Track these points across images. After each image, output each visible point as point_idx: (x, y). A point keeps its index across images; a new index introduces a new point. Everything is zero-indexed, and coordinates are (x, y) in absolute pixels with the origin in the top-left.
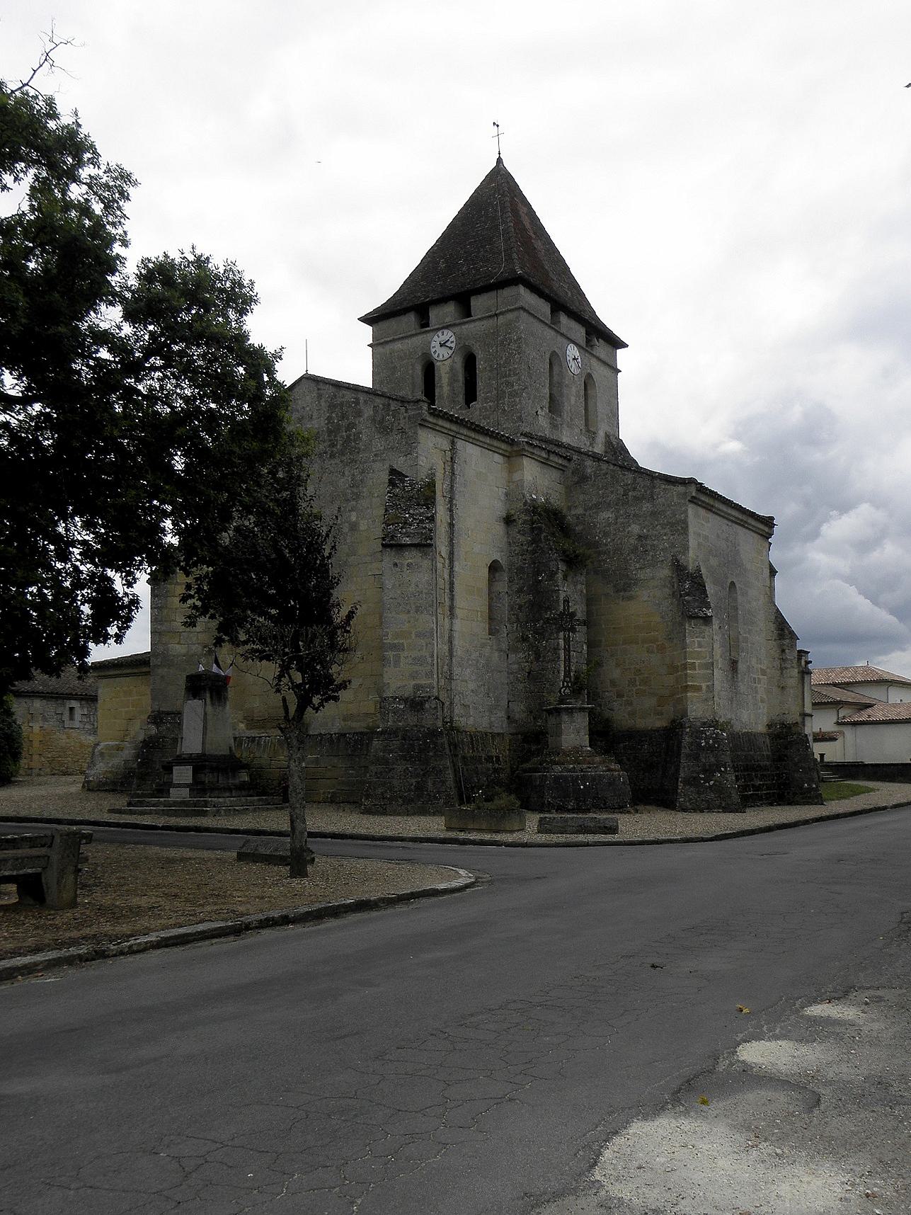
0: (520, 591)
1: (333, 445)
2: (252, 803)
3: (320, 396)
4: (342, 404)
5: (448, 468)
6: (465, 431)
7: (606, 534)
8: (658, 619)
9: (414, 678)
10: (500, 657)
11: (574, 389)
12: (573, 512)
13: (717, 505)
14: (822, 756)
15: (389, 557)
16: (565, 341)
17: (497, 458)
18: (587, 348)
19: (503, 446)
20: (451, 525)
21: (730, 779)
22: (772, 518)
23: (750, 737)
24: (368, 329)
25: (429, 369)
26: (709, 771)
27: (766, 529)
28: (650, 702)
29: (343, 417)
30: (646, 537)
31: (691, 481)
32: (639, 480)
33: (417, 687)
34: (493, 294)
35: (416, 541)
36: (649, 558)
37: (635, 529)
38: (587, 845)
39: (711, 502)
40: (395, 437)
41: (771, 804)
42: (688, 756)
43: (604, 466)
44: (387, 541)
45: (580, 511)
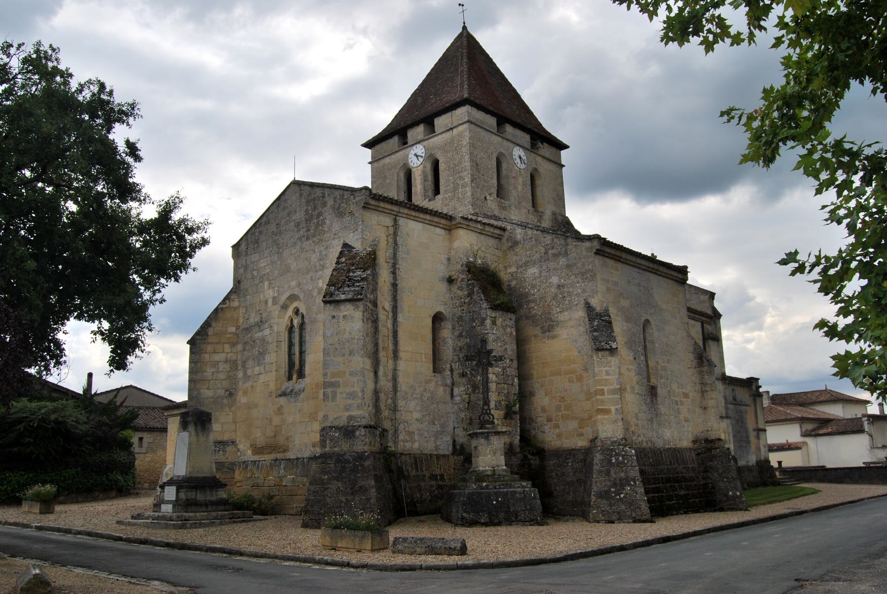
0: (460, 336)
1: (308, 230)
2: (222, 517)
3: (301, 195)
4: (314, 199)
5: (391, 240)
6: (406, 211)
7: (533, 286)
8: (576, 353)
9: (347, 410)
10: (445, 391)
11: (520, 180)
12: (509, 271)
13: (624, 255)
14: (780, 463)
15: (330, 309)
16: (511, 145)
17: (439, 231)
18: (533, 148)
19: (443, 221)
20: (394, 285)
21: (639, 493)
22: (686, 267)
23: (675, 452)
24: (368, 152)
25: (409, 174)
26: (621, 484)
27: (680, 276)
28: (573, 425)
29: (315, 208)
30: (563, 286)
31: (597, 237)
32: (556, 240)
33: (351, 418)
34: (448, 115)
35: (350, 296)
36: (567, 302)
37: (555, 280)
38: (412, 568)
39: (618, 253)
40: (347, 218)
41: (686, 513)
42: (600, 472)
43: (529, 232)
44: (327, 299)
45: (513, 269)
